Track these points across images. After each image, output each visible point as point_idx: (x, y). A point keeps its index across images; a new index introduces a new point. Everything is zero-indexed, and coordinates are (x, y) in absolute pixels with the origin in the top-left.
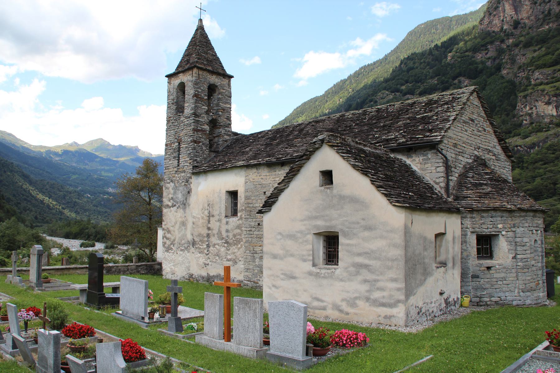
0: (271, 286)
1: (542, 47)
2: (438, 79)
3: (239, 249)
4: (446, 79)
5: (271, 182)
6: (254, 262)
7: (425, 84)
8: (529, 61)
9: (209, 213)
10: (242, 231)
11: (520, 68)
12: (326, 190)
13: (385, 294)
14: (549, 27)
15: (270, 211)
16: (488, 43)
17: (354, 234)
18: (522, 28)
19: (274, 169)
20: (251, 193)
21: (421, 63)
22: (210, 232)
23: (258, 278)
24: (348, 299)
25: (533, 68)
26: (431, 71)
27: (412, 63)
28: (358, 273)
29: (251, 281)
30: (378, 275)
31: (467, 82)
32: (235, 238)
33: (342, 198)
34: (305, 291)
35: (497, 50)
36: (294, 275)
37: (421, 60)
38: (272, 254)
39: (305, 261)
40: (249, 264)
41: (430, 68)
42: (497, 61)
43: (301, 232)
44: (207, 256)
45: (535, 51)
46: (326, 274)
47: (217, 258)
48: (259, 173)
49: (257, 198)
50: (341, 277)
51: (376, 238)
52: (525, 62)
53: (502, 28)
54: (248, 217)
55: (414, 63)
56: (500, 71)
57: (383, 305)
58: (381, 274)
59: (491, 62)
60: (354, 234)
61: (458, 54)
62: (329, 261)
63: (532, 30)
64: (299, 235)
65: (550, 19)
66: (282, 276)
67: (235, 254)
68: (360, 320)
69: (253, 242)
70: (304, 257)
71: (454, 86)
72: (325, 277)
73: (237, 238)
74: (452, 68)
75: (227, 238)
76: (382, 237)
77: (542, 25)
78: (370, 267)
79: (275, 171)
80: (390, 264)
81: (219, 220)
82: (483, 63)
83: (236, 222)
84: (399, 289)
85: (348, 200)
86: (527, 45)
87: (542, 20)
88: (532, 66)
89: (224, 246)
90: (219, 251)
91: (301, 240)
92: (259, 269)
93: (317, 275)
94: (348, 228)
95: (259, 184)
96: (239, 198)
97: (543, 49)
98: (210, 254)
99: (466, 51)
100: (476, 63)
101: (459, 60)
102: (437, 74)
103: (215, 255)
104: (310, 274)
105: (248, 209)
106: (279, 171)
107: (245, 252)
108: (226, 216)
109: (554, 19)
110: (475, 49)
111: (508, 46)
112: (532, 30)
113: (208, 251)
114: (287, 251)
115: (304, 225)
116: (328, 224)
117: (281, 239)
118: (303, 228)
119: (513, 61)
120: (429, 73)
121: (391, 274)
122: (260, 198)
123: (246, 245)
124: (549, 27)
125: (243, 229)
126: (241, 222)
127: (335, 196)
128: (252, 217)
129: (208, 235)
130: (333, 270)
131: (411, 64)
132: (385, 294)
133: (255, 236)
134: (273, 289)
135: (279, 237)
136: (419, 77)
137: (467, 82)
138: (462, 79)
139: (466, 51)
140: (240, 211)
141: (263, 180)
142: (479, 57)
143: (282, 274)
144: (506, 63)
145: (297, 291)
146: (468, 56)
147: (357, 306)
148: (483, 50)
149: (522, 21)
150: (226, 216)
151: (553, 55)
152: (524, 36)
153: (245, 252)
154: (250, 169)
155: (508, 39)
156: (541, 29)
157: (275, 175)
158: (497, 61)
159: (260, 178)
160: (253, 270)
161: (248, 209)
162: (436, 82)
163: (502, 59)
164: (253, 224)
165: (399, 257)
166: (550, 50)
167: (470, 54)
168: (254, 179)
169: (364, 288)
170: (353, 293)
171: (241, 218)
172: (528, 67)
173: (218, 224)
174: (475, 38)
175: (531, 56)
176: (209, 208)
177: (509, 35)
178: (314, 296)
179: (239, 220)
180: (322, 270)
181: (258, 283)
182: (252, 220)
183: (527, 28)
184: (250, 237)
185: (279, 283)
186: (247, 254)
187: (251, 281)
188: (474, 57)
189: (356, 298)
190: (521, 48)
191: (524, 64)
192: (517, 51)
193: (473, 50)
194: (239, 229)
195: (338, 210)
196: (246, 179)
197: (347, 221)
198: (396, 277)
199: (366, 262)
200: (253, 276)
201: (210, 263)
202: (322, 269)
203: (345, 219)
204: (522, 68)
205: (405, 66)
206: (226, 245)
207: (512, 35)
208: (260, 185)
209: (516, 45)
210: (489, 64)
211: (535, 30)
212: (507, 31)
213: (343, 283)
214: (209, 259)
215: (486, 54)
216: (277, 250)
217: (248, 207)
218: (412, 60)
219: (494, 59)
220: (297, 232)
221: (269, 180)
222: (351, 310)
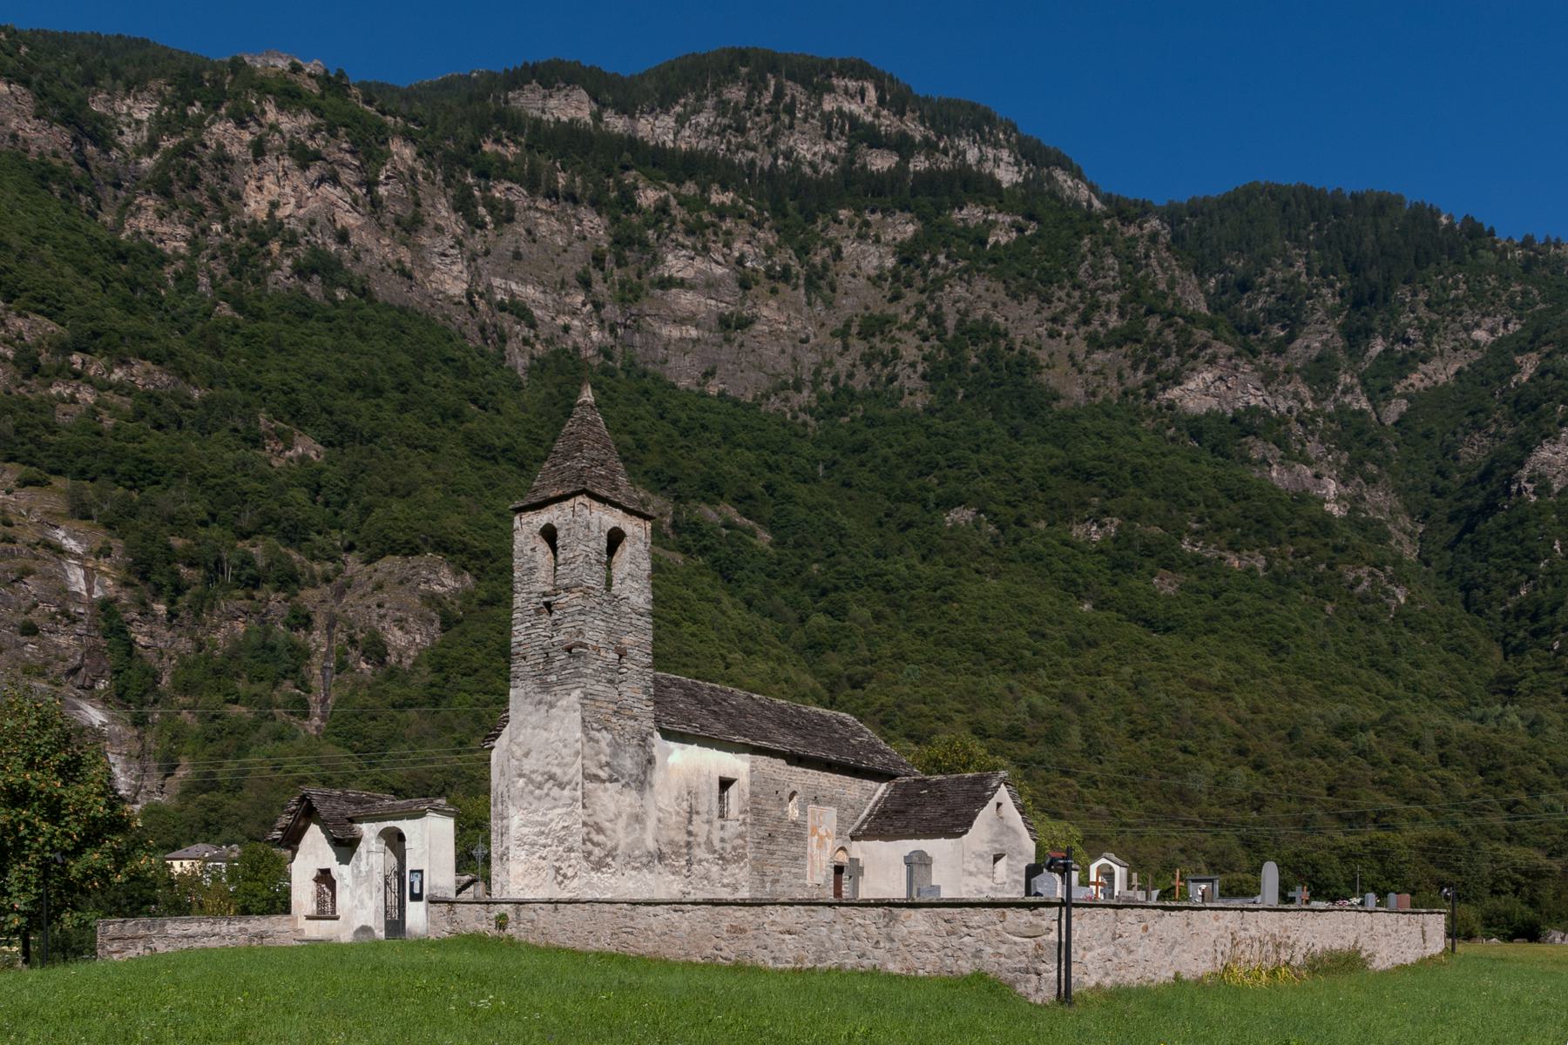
3: (741, 869)
6: (764, 887)
22: (691, 839)
47: (706, 882)
81: (709, 822)
90: (709, 870)
126: (743, 828)
129: (688, 845)
173: (706, 827)
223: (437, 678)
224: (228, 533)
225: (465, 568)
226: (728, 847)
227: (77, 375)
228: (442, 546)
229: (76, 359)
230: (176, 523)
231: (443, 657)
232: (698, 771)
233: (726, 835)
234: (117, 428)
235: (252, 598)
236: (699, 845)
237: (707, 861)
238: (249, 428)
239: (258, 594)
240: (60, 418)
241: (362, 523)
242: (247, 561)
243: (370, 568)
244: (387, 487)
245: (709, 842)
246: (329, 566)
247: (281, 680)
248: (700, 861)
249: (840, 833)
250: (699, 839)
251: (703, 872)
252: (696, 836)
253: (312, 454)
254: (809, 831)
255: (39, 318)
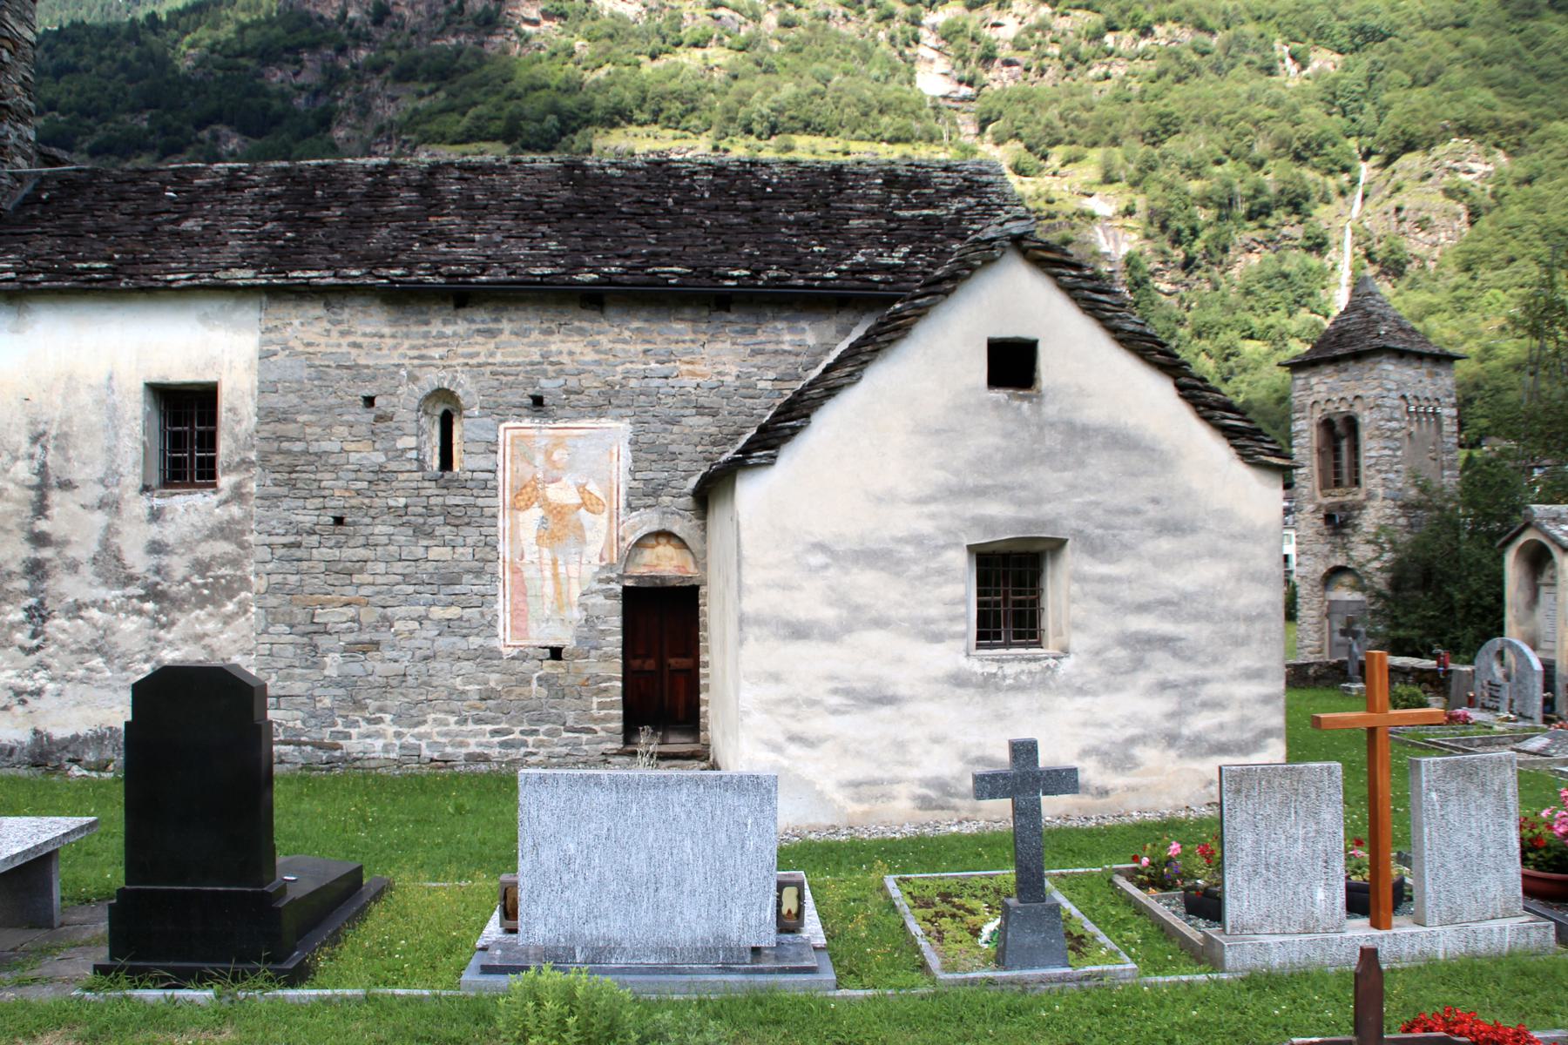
0: (781, 739)
1: (438, 89)
2: (152, 116)
3: (228, 620)
4: (176, 124)
5: (406, 361)
6: (317, 665)
7: (111, 125)
8: (406, 117)
9: (43, 471)
10: (242, 545)
11: (380, 130)
12: (1017, 403)
13: (1227, 716)
14: (459, 43)
15: (772, 464)
16: (303, 45)
17: (1125, 546)
18: (395, 26)
19: (422, 313)
20: (293, 399)
21: (101, 59)
22: (47, 553)
23: (340, 728)
24: (1106, 747)
25: (414, 137)
26: (130, 88)
27: (71, 51)
28: (1138, 664)
29: (299, 744)
30: (1204, 665)
31: (235, 141)
32: (203, 576)
33: (1078, 432)
34: (936, 740)
35: (324, 70)
36: (890, 692)
37: (102, 47)
38: (787, 624)
39: (937, 638)
40: (289, 677)
41: (131, 81)
42: (323, 101)
43: (918, 540)
44: (33, 658)
45: (421, 95)
46: (1024, 677)
47: (97, 661)
48: (340, 322)
49: (328, 420)
50: (1078, 682)
51: (1198, 556)
52: (396, 118)
53: (344, 14)
54: (284, 490)
55: (79, 54)
56: (329, 130)
57: (1222, 749)
58: (1215, 660)
59: (307, 100)
60: (1125, 546)
61: (216, 56)
62: (1033, 635)
63: (418, 39)
64: (909, 550)
65: (461, 23)
66: (835, 701)
67: (207, 641)
68: (1149, 802)
69: (307, 589)
70: (933, 627)
71: (199, 146)
72: (1018, 688)
73: (217, 578)
74: (196, 94)
75: (157, 579)
76: (1214, 553)
77: (441, 32)
78: (1179, 644)
79: (427, 323)
80: (1241, 629)
81: (110, 505)
82: (284, 96)
83: (211, 514)
84: (1267, 700)
85: (1100, 439)
86: (405, 74)
87: (443, 21)
88: (413, 132)
89: (140, 612)
90: (108, 630)
91: (916, 569)
92: (341, 692)
93: (988, 684)
94: (1101, 526)
95: (339, 367)
96: (223, 414)
97: (442, 95)
98: (52, 649)
99: (242, 54)
100: (267, 94)
101: (220, 74)
102: (149, 102)
103: (83, 650)
104: (959, 680)
105: (277, 459)
106: (445, 323)
107: (265, 632)
108: (146, 489)
109: (471, 25)
110: (267, 55)
111: (354, 67)
112: (418, 39)
113: (34, 635)
114: (857, 608)
115: (932, 516)
116: (1028, 513)
117: (826, 567)
118: (926, 527)
119: (365, 110)
120: (125, 94)
121: (1246, 659)
122: (345, 418)
123: (272, 601)
124: (459, 43)
125: (251, 538)
126: (235, 510)
127: (1052, 425)
128: (304, 493)
129: (36, 569)
130: (1051, 662)
131: (68, 55)
132: (1227, 716)
133: (322, 566)
134: (794, 749)
135: (817, 559)
136: (90, 100)
137: (235, 141)
138: (223, 130)
139: (242, 54)
140: (229, 469)
141: (362, 352)
142: (276, 77)
143: (835, 692)
144: (347, 110)
145: (900, 746)
146: (246, 69)
147: (1137, 765)
148: (287, 61)
149: (395, 10)
150: (146, 489)
151: (464, 114)
152: (399, 50)
153: (265, 632)
154: (290, 305)
155: (357, 47)
156: (438, 43)
157: (426, 335)
158: (323, 101)
159: (345, 341)
160: (312, 697)
161: (277, 459)
162: (145, 125)
163: (336, 98)
164: (307, 519)
165: (1269, 610)
166: (457, 102)
167: (250, 63)
168: (309, 344)
169: (1156, 708)
170: (1123, 726)
171: (238, 495)
172: (401, 132)
173: (100, 518)
174: (270, 21)
175: (410, 106)
176: (38, 450)
177: (360, 38)
178: (975, 753)
179: (225, 502)
180: (1006, 666)
181: (337, 747)
182: (300, 503)
183: (407, 31)
184: (293, 569)
185: (818, 724)
186: (275, 639)
187: (299, 744)
188: (262, 76)
189: (1132, 741)
190: (387, 78)
191: (391, 122)
192: (376, 84)
193: (261, 56)
194: (226, 538)
195: (1065, 469)
196: (263, 343)
197: (1097, 504)
198: (1259, 665)
199: (1167, 628)
200: (313, 721)
201: (51, 686)
202: (1008, 661)
203: (1092, 498)
204: (387, 132)
205: (47, 57)
206: (149, 606)
207: (368, 38)
208: (348, 368)
209: (377, 69)
210: (300, 102)
211: (425, 40)
212: (357, 25)
213: (1088, 699)
214: (47, 667)
215: (296, 74)
216: (809, 604)
217: (280, 452)
218: (73, 42)
219: (316, 94)
220: (900, 540)
221: (396, 354)
222: (1115, 781)
223: (1464, 278)
224: (1243, 165)
225: (1497, 145)
226: (178, 565)
227: (1110, 53)
228: (1467, 129)
229: (1109, 39)
230: (1193, 169)
231: (1471, 252)
232: (71, 383)
233: (168, 533)
234: (1144, 91)
235: (1263, 227)
236: (73, 567)
237: (103, 606)
238: (1264, 57)
239: (1271, 222)
240: (1095, 96)
241: (1380, 122)
242: (1258, 191)
243: (1388, 171)
244: (1407, 80)
245: (110, 564)
246: (1345, 178)
247: (1295, 307)
248: (76, 609)
249: (645, 494)
250: (71, 552)
251: (88, 634)
252: (64, 543)
253: (1329, 66)
254: (505, 496)
255: (1078, 13)
